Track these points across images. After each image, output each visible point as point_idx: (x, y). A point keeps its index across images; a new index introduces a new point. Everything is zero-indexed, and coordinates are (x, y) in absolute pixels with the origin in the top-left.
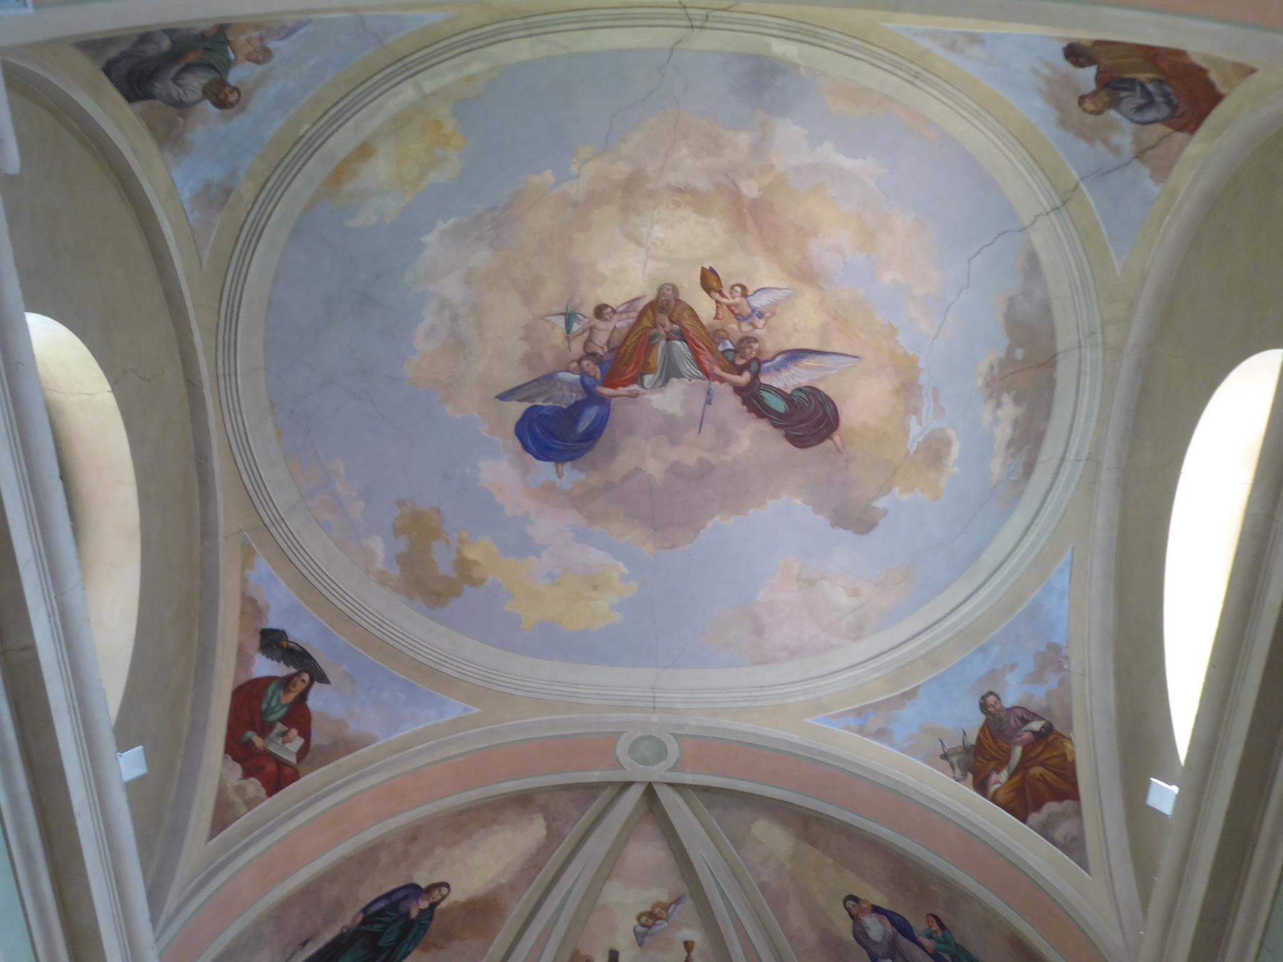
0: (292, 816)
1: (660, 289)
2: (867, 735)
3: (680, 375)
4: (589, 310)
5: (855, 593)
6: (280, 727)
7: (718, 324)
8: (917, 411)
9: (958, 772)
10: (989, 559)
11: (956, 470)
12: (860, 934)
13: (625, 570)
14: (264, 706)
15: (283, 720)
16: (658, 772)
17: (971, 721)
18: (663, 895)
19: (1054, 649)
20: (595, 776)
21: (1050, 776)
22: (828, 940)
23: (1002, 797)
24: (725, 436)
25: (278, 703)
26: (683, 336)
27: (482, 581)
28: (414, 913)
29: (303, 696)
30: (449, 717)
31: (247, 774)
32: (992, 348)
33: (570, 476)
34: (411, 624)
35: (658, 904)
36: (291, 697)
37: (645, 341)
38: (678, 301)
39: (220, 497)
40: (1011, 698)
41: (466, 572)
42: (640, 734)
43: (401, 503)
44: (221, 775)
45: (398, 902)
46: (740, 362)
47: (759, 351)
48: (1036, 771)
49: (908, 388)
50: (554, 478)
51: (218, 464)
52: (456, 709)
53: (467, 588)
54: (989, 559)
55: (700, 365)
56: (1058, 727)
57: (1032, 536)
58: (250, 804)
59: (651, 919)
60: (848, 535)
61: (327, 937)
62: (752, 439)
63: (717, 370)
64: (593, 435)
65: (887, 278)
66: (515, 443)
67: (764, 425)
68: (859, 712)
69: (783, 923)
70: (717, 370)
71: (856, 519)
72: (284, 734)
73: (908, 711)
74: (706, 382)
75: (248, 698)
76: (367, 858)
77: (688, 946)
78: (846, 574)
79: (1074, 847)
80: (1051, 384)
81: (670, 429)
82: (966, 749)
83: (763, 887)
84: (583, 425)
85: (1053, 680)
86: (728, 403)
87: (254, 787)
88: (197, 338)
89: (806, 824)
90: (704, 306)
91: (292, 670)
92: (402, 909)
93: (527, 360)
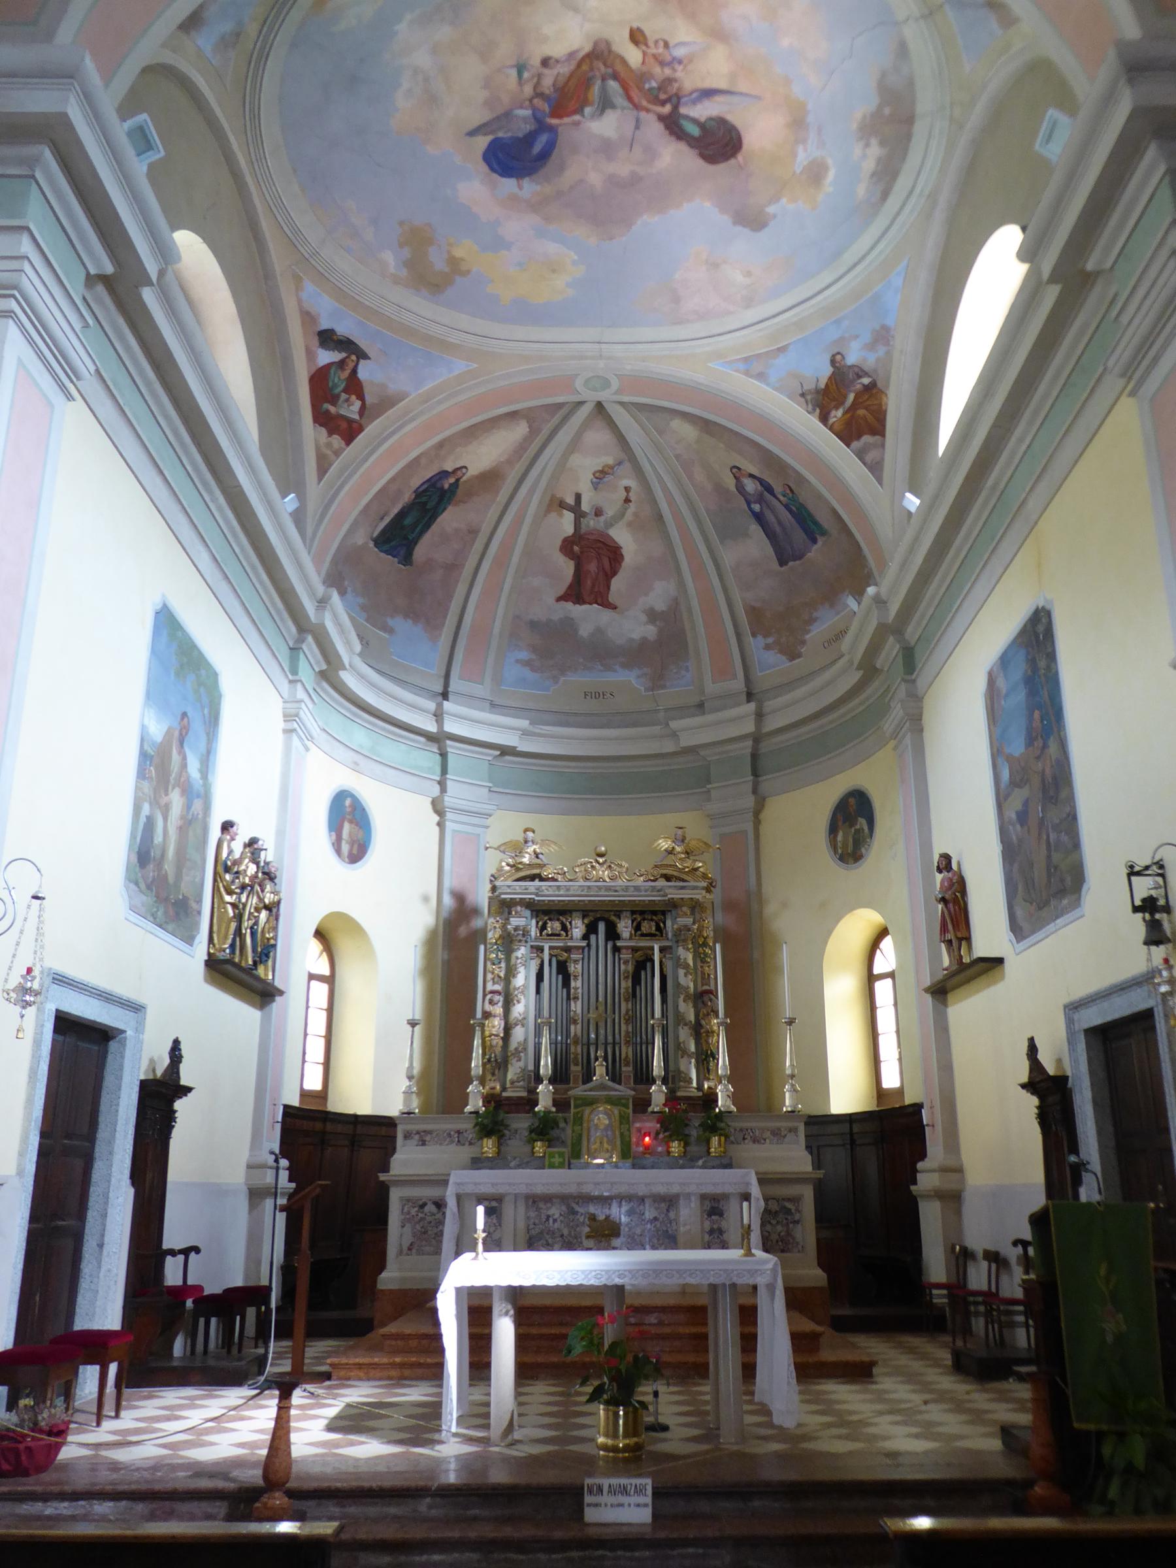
0: (366, 460)
1: (596, 44)
2: (751, 377)
3: (613, 107)
4: (536, 61)
5: (749, 274)
6: (344, 396)
7: (645, 69)
8: (804, 141)
9: (810, 407)
10: (849, 257)
11: (831, 189)
12: (740, 488)
13: (576, 257)
14: (331, 384)
15: (345, 391)
16: (604, 396)
17: (819, 371)
18: (610, 461)
19: (885, 328)
20: (560, 399)
21: (869, 417)
22: (719, 489)
23: (836, 427)
24: (651, 154)
25: (339, 379)
26: (615, 77)
27: (468, 272)
28: (446, 486)
29: (354, 371)
30: (456, 372)
31: (330, 433)
32: (865, 104)
33: (528, 188)
34: (419, 309)
35: (607, 466)
36: (347, 373)
37: (586, 81)
38: (610, 51)
39: (271, 245)
40: (852, 359)
41: (456, 267)
42: (592, 374)
43: (401, 223)
44: (316, 441)
45: (435, 483)
46: (663, 96)
47: (679, 89)
48: (861, 412)
49: (798, 123)
50: (516, 190)
51: (265, 224)
52: (460, 366)
53: (458, 279)
54: (849, 257)
55: (629, 98)
56: (879, 385)
57: (881, 246)
58: (337, 453)
59: (601, 476)
60: (746, 231)
61: (396, 511)
62: (672, 156)
63: (644, 103)
64: (545, 156)
65: (785, 42)
66: (485, 168)
67: (682, 147)
68: (746, 360)
69: (690, 477)
70: (644, 103)
71: (752, 220)
72: (347, 400)
73: (781, 361)
74: (635, 112)
75: (319, 380)
76: (414, 464)
77: (627, 489)
78: (745, 258)
79: (876, 469)
80: (909, 137)
81: (607, 148)
82: (817, 391)
83: (677, 457)
84: (537, 148)
85: (881, 351)
86: (654, 129)
87: (337, 441)
88: (235, 146)
89: (707, 426)
90: (633, 56)
91: (344, 355)
92: (439, 485)
93: (489, 103)
